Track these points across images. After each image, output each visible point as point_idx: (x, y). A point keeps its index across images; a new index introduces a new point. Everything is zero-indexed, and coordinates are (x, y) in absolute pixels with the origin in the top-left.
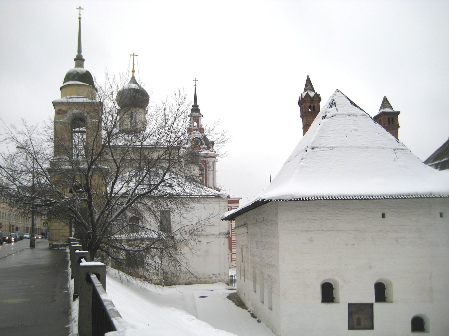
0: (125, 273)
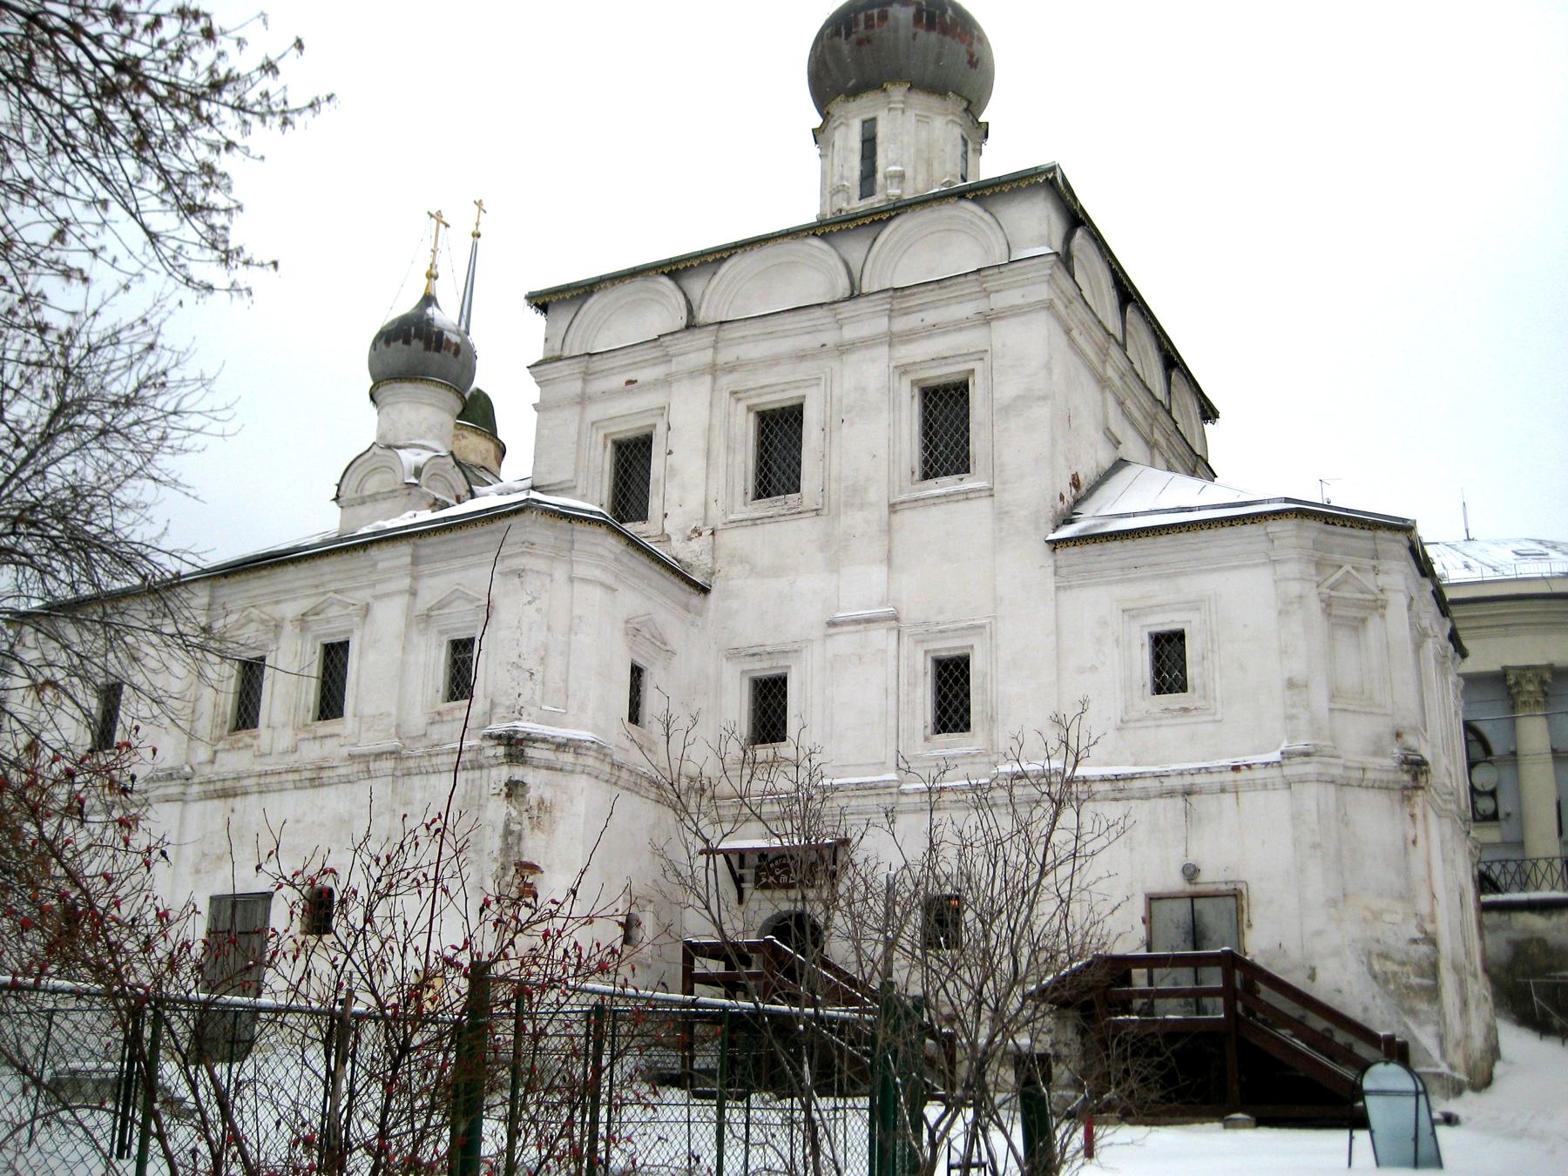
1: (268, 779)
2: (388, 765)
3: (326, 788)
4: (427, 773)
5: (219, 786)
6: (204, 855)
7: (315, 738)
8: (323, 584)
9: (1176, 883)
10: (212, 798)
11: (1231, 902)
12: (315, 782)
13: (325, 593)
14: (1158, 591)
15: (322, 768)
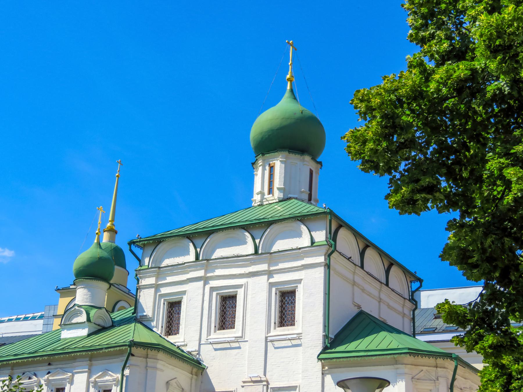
0: (75, 321)
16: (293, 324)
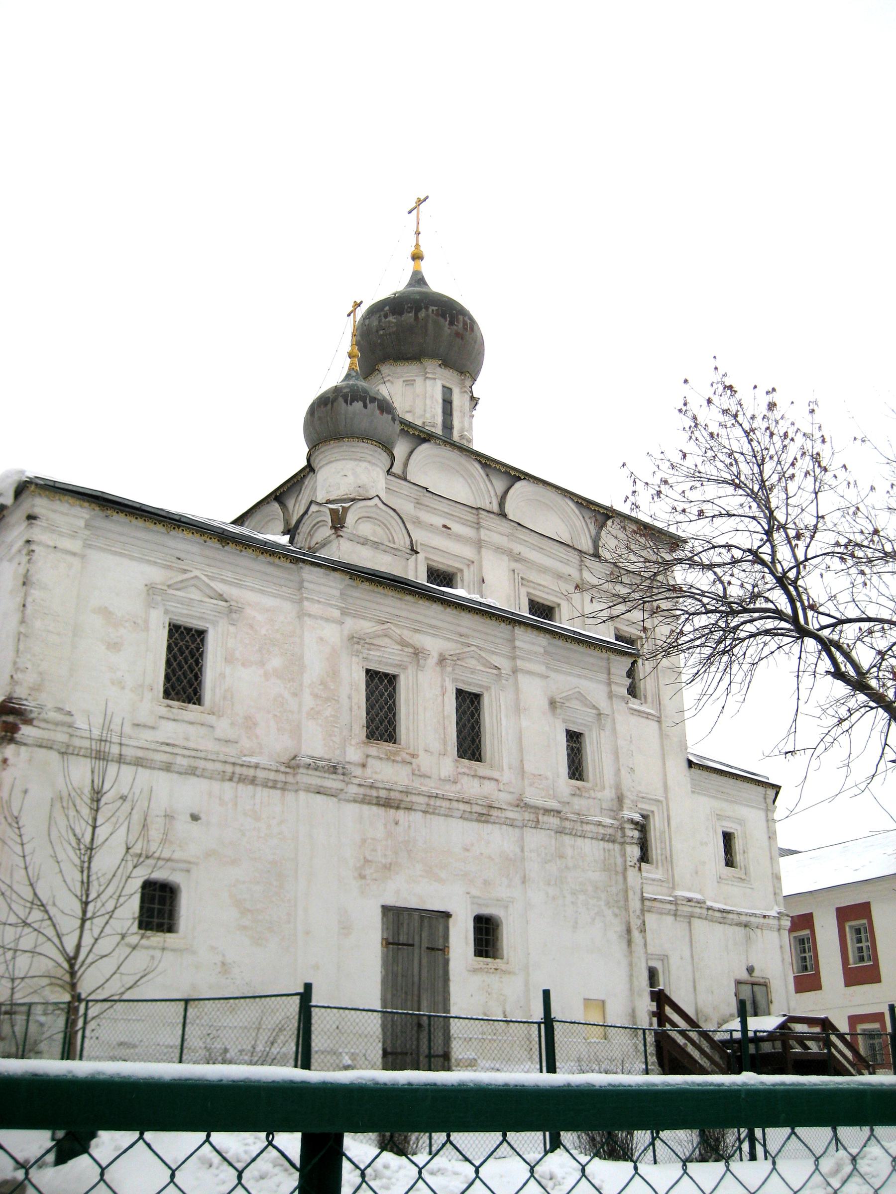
1: (438, 802)
2: (554, 821)
3: (490, 826)
4: (575, 835)
5: (383, 794)
6: (367, 861)
7: (474, 776)
8: (467, 636)
9: (744, 976)
10: (369, 803)
11: (764, 988)
12: (483, 818)
13: (469, 645)
14: (729, 809)
15: (491, 807)
16: (797, 992)
